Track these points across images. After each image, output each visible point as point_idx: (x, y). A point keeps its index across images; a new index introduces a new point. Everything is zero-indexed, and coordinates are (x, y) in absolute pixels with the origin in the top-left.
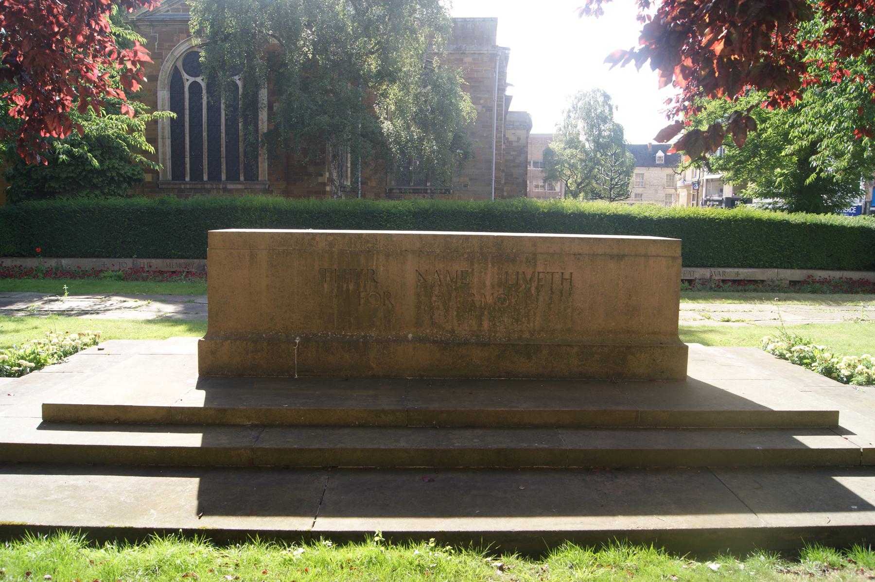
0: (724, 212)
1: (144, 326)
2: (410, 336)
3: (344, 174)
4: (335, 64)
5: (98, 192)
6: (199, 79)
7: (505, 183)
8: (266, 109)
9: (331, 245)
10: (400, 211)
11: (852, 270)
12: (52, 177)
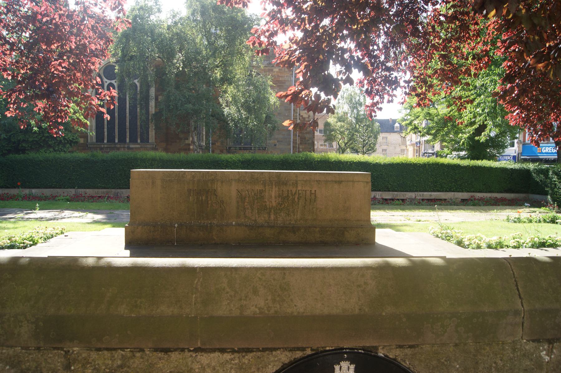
0: (433, 159)
1: (87, 225)
2: (234, 223)
3: (201, 139)
4: (196, 74)
5: (51, 150)
6: (113, 82)
7: (301, 143)
8: (154, 100)
9: (194, 177)
10: (234, 160)
11: (498, 192)
12: (24, 141)
